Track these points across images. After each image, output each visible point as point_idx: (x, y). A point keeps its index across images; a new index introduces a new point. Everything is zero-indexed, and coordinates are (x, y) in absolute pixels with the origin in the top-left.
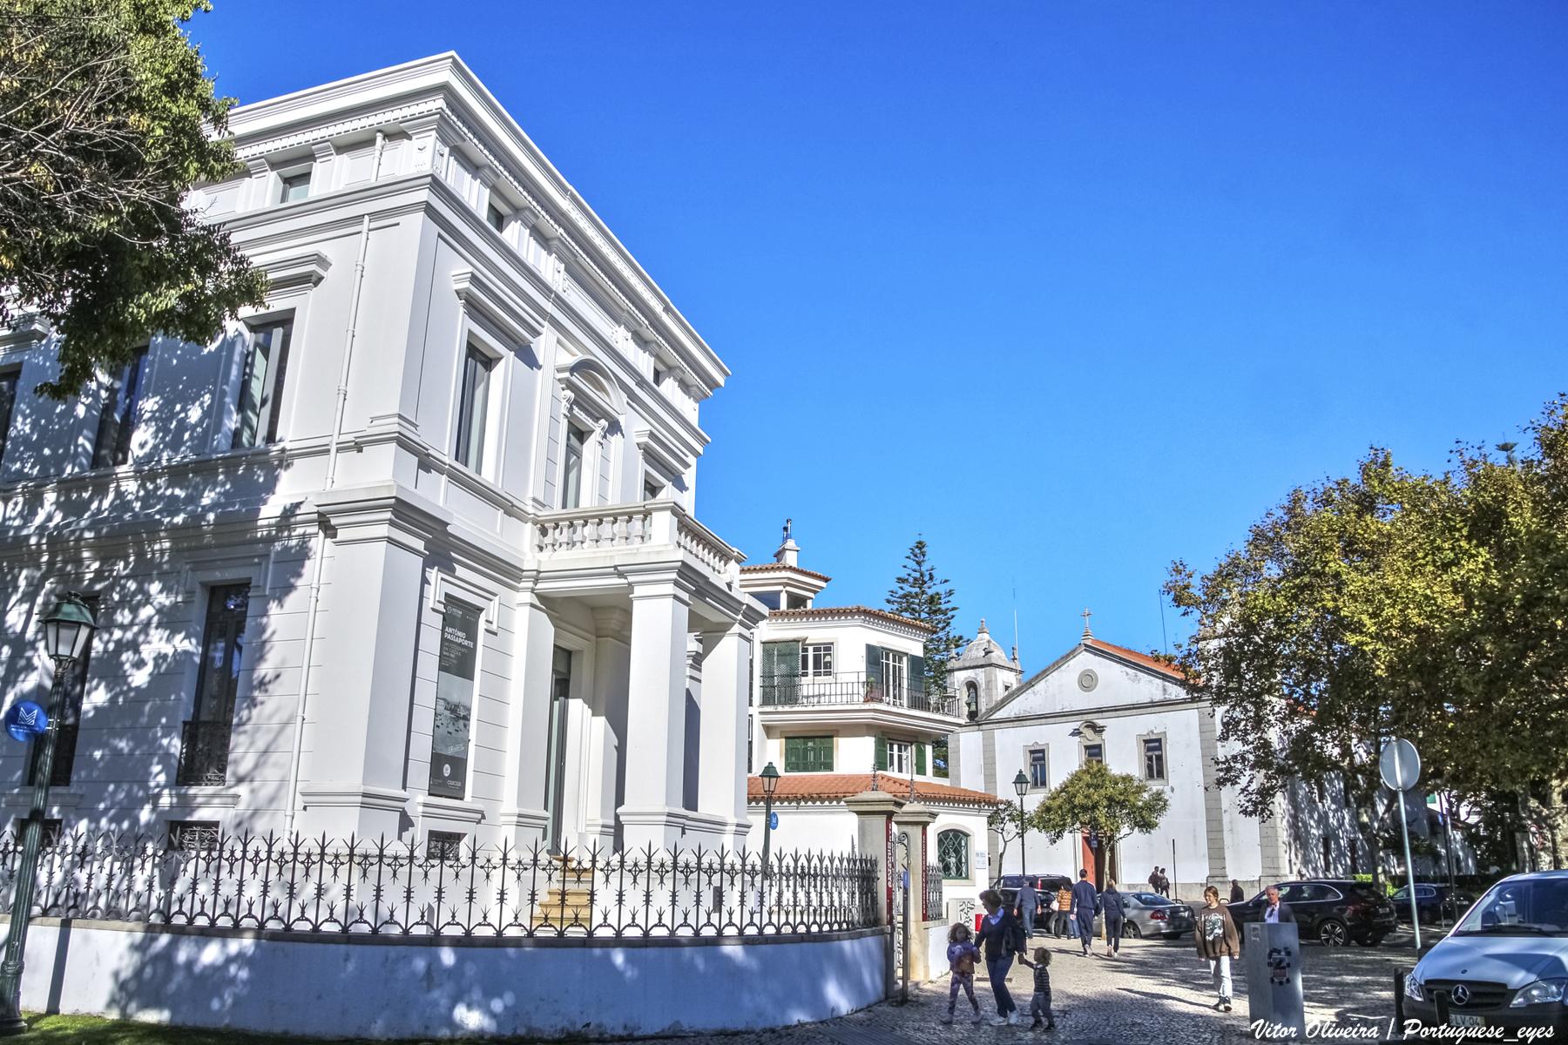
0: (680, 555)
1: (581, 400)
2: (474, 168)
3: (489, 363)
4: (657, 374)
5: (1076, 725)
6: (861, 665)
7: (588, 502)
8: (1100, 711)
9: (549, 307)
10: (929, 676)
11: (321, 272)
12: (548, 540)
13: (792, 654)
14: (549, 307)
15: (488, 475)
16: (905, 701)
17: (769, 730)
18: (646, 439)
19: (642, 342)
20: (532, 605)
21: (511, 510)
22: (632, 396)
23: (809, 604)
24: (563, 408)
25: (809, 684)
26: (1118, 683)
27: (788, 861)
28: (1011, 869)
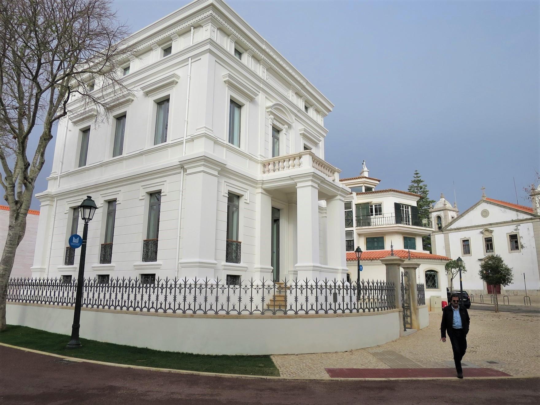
0: (313, 170)
1: (277, 118)
2: (227, 34)
3: (240, 106)
4: (306, 108)
5: (481, 230)
6: (393, 210)
7: (283, 153)
8: (491, 224)
9: (261, 86)
10: (419, 215)
11: (177, 80)
12: (266, 169)
13: (367, 208)
14: (261, 86)
15: (243, 148)
16: (411, 223)
17: (360, 235)
18: (303, 132)
19: (298, 94)
20: (262, 193)
21: (251, 159)
22: (296, 116)
23: (373, 190)
24: (270, 122)
25: (374, 219)
26: (497, 214)
27: (366, 284)
28: (456, 287)
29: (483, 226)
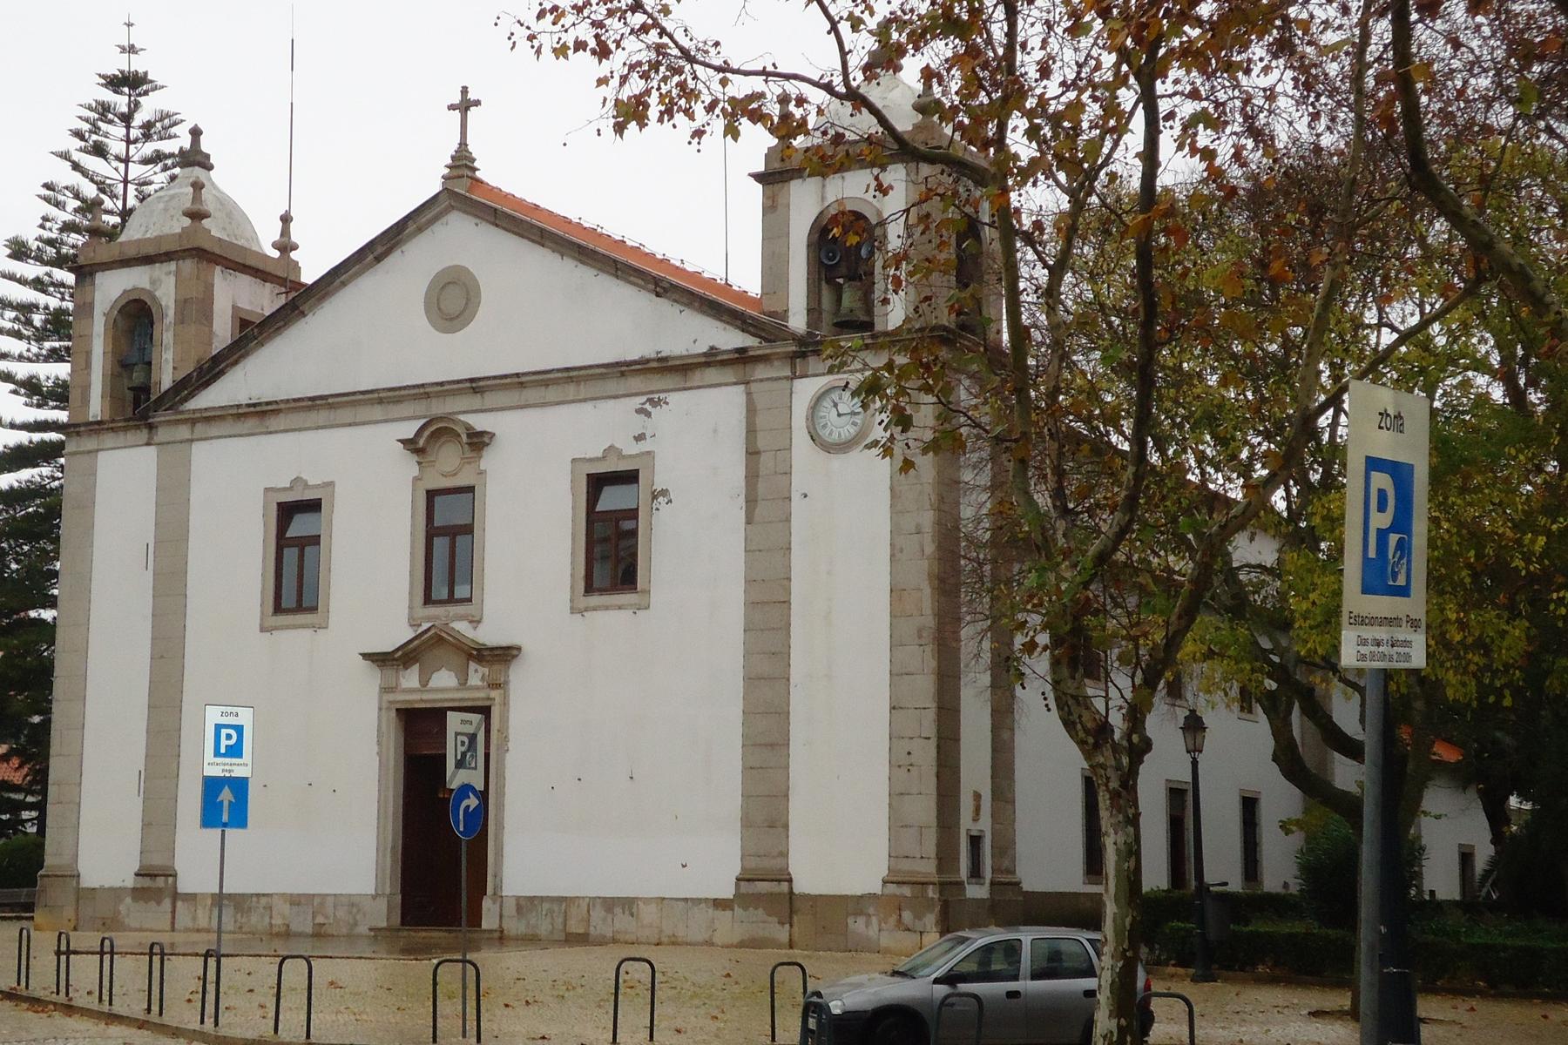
8: (475, 386)
29: (422, 392)
